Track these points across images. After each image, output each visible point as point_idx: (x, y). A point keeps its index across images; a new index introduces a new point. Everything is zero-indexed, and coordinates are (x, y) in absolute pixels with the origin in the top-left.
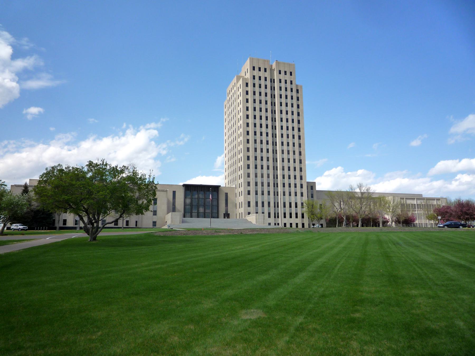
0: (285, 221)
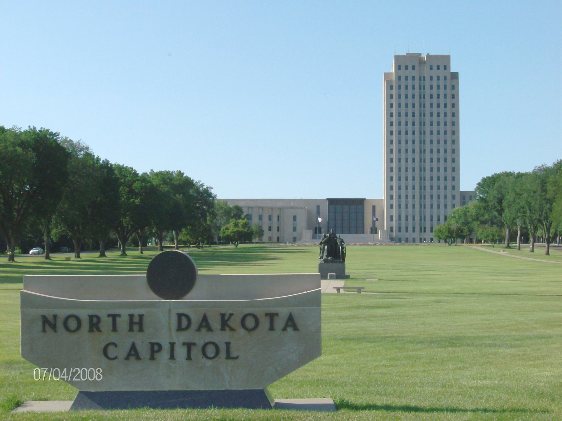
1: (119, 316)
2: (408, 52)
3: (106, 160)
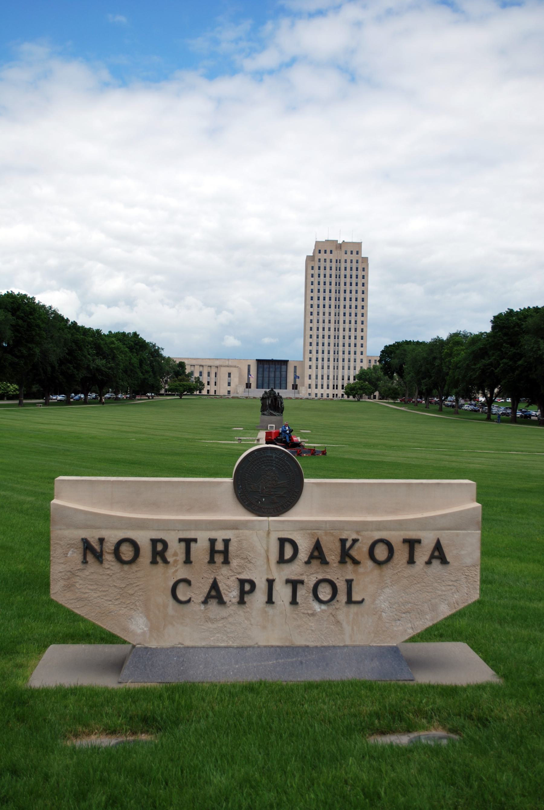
0: (316, 391)
1: (195, 540)
2: (327, 239)
3: (74, 321)
